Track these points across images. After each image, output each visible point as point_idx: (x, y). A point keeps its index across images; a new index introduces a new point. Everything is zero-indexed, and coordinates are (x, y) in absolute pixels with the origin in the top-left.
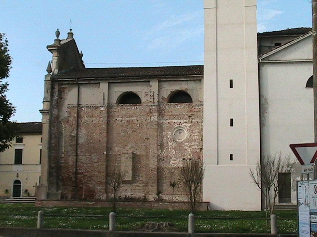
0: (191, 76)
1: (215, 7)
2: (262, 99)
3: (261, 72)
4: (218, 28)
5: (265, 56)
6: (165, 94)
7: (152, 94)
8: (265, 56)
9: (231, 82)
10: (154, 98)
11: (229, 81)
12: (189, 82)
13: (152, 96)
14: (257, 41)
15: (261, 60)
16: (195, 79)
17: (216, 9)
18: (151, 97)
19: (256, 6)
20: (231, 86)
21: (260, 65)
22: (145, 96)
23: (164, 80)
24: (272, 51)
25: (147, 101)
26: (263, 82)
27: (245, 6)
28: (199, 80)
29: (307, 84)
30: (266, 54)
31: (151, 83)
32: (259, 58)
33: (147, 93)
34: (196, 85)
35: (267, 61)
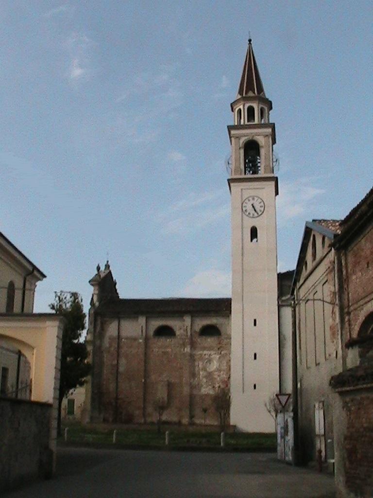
21: (279, 307)
31: (184, 318)
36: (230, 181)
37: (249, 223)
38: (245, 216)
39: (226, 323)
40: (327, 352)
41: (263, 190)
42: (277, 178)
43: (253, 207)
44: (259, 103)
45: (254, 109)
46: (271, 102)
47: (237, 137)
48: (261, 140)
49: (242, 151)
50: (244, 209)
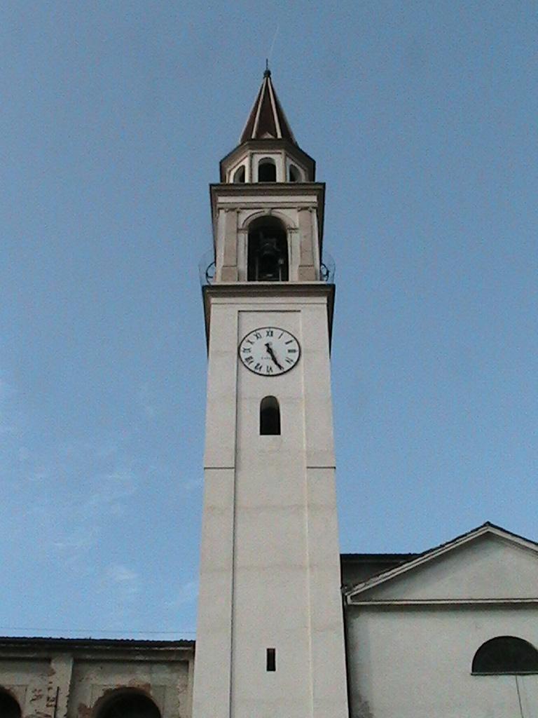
0: (162, 649)
1: (233, 466)
2: (357, 705)
3: (350, 630)
4: (239, 515)
5: (360, 588)
6: (89, 698)
7: (52, 694)
8: (362, 588)
9: (271, 654)
10: (56, 706)
11: (266, 651)
12: (155, 667)
13: (51, 699)
14: (339, 570)
15: (351, 598)
16: (173, 658)
17: (235, 472)
18: (50, 704)
19: (335, 468)
20: (271, 666)
21: (349, 612)
22: (33, 700)
23: (88, 656)
24: (378, 576)
25: (38, 713)
26: (360, 656)
27: (308, 468)
28: (184, 661)
29: (478, 651)
30: (364, 584)
31: (53, 665)
32: (346, 594)
33: (40, 690)
34: (175, 675)
35: (365, 601)
36: (209, 291)
37: (258, 389)
38: (246, 374)
39: (179, 683)
40: (248, 337)
41: (299, 314)
42: (333, 287)
43: (270, 351)
44: (286, 155)
45: (274, 167)
46: (314, 162)
47: (233, 210)
48: (291, 218)
49: (244, 238)
50: (244, 356)
